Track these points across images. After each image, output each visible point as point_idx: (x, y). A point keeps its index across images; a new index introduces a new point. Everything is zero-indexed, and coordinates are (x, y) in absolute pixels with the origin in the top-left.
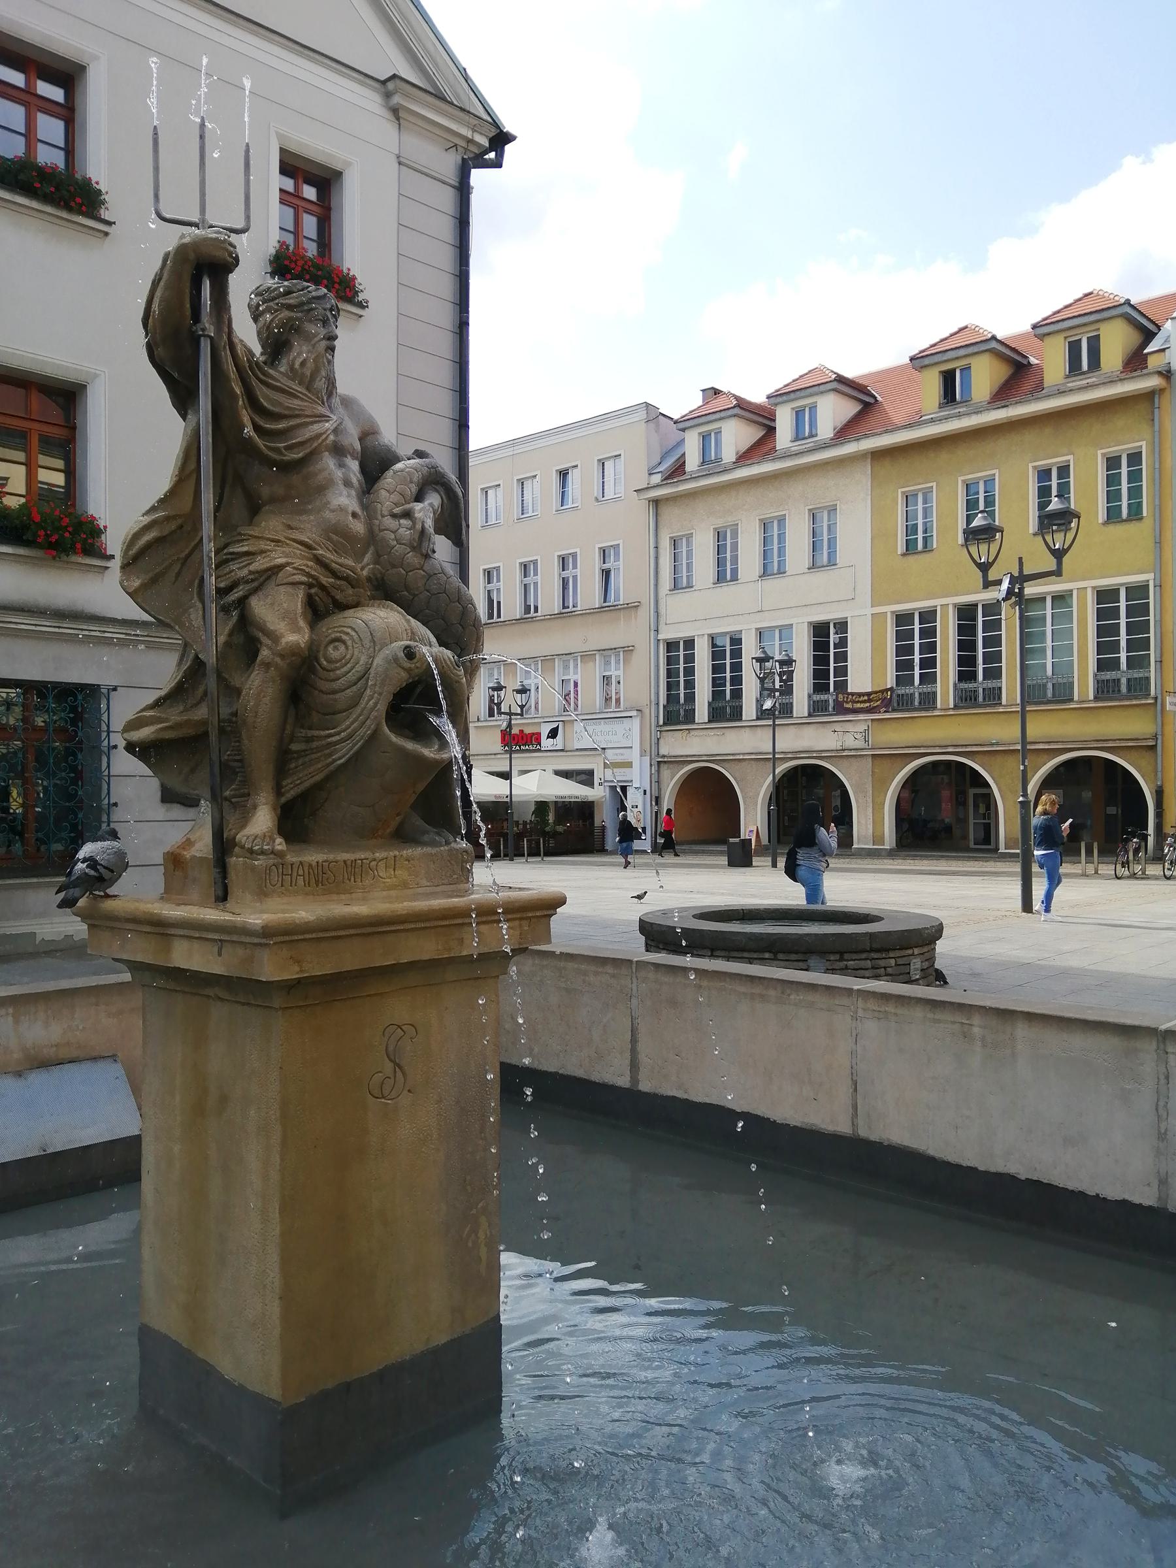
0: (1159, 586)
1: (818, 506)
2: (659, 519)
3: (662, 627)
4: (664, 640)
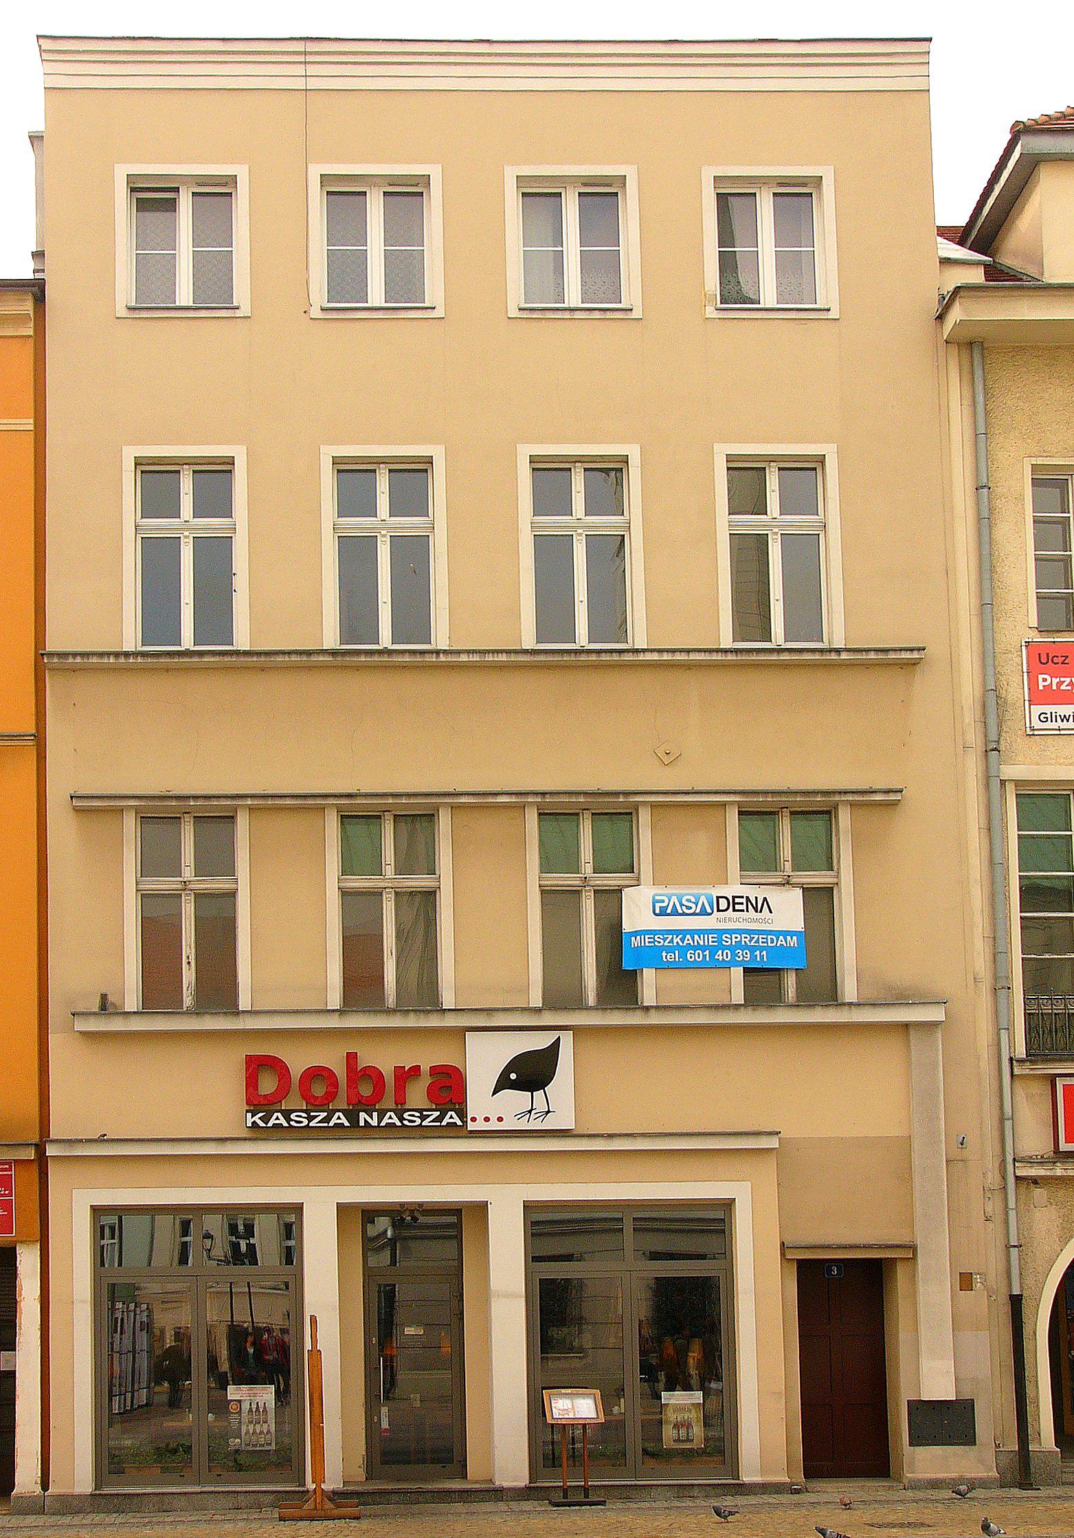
3: (1013, 740)
4: (1018, 783)
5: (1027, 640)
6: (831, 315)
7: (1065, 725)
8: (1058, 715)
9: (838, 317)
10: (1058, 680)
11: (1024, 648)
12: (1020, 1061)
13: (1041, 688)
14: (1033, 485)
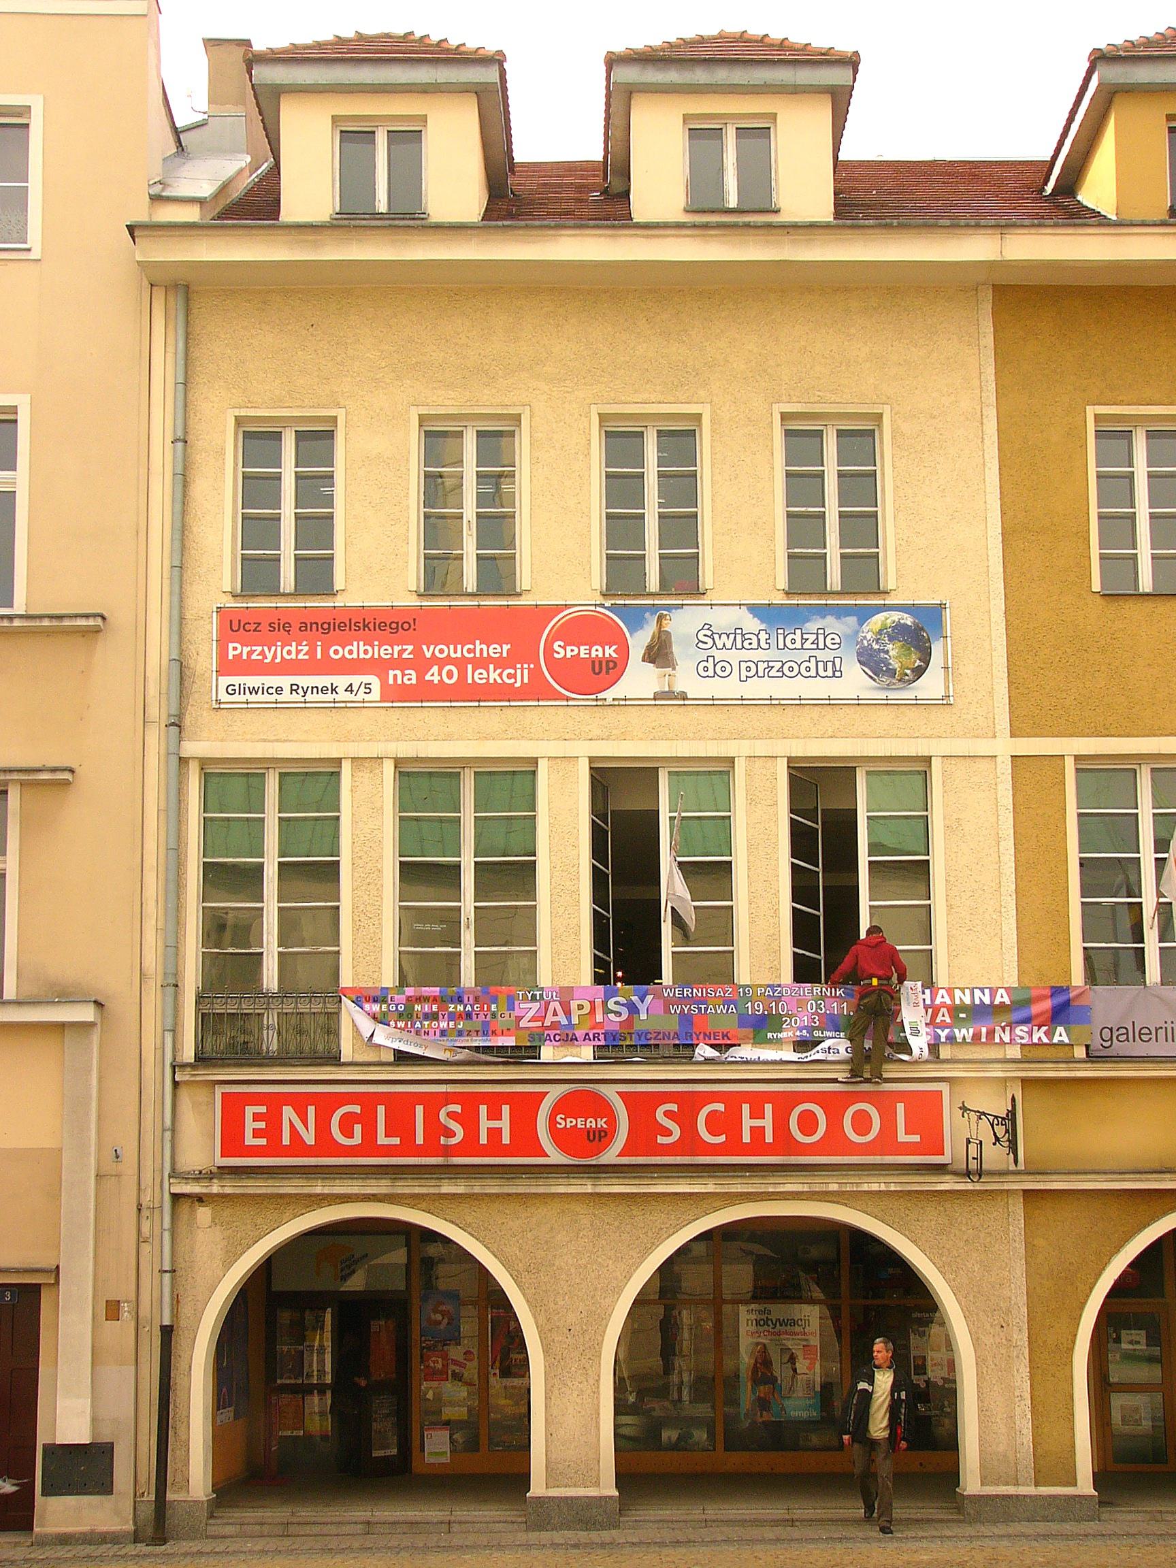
0: (917, 703)
1: (818, 409)
2: (195, 353)
3: (197, 714)
4: (204, 762)
5: (219, 606)
6: (32, 256)
7: (253, 698)
8: (246, 687)
9: (39, 258)
10: (249, 648)
11: (215, 614)
12: (184, 1066)
13: (230, 657)
14: (1097, 437)
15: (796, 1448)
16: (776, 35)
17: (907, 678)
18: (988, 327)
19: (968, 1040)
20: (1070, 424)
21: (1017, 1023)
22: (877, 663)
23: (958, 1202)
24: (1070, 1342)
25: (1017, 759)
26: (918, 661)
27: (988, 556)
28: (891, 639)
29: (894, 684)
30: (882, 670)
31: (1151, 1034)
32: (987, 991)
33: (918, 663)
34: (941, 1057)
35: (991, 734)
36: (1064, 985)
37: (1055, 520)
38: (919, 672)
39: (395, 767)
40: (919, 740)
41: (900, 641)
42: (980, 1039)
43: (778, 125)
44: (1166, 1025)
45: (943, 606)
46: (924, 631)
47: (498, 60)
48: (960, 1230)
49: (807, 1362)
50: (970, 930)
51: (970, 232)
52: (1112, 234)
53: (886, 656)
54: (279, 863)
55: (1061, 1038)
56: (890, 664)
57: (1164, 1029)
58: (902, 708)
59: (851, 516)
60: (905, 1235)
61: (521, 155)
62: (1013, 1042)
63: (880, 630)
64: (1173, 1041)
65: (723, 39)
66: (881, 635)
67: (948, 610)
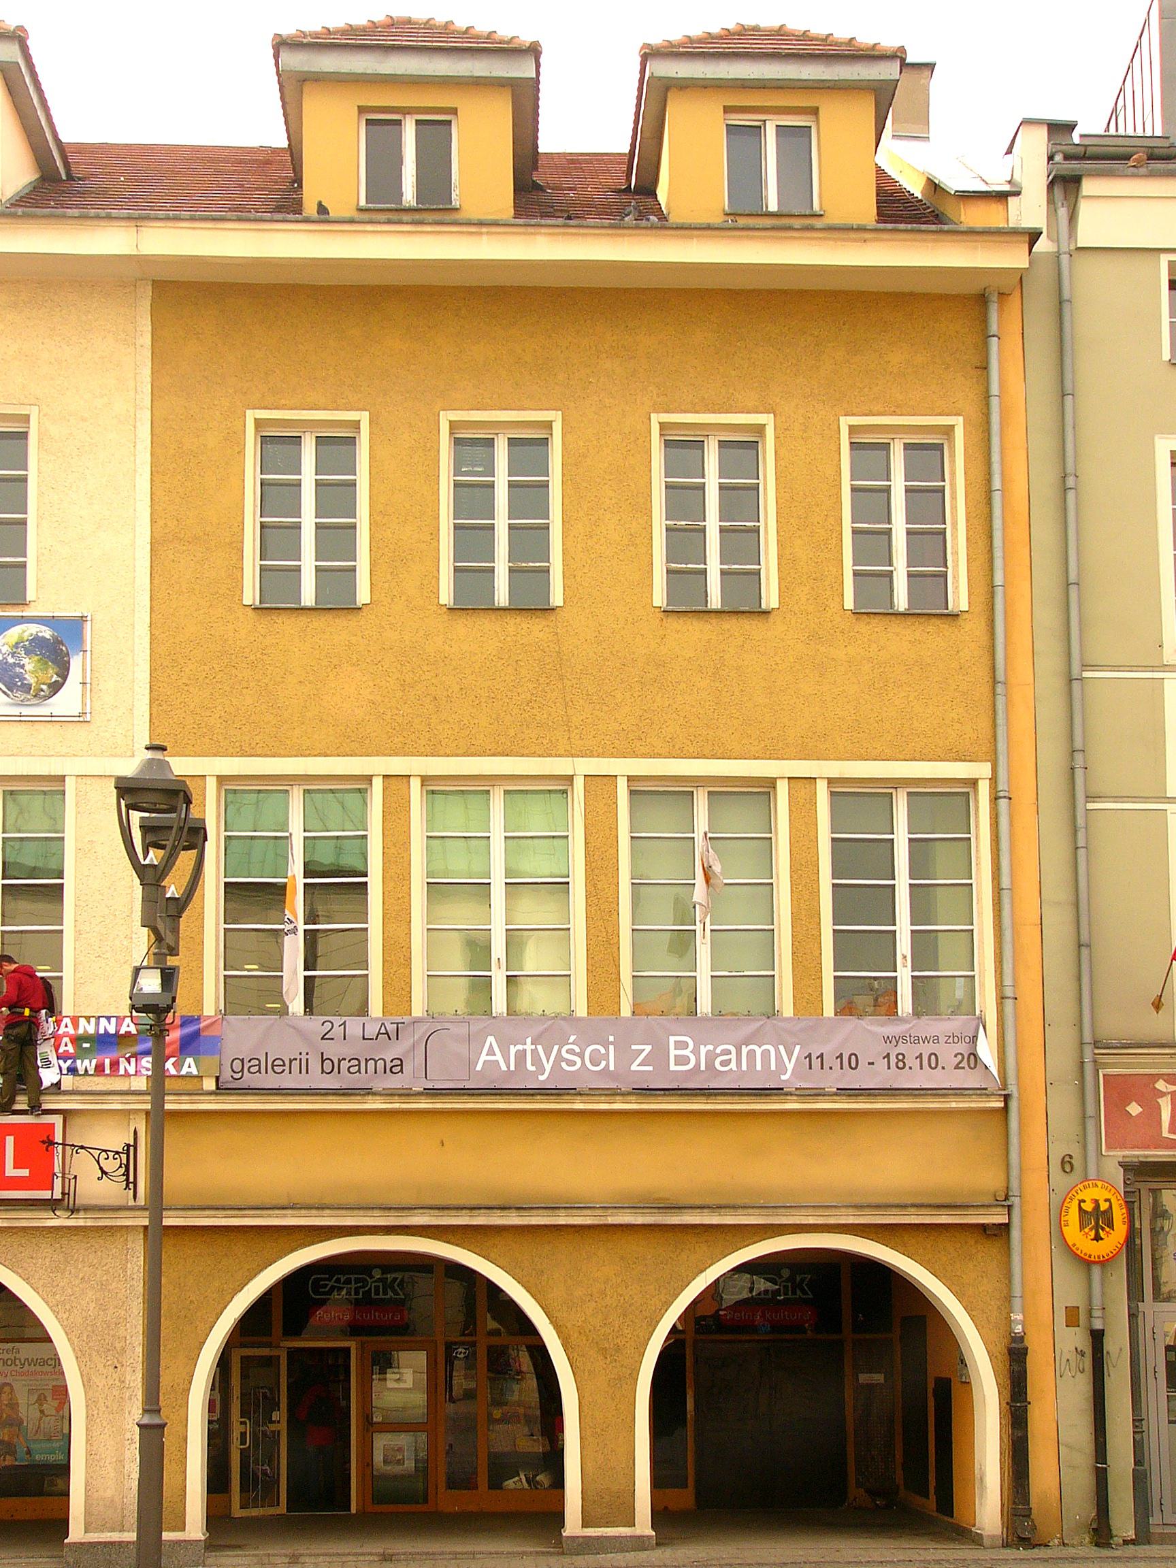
0: (52, 720)
14: (851, 449)
15: (41, 1493)
16: (461, 24)
17: (42, 693)
18: (145, 325)
19: (91, 1072)
20: (229, 428)
21: (141, 1054)
22: (12, 678)
23: (76, 1238)
24: (186, 1382)
25: (393, 780)
26: (55, 676)
27: (135, 567)
28: (28, 652)
29: (29, 700)
30: (15, 685)
31: (284, 1065)
32: (113, 1020)
33: (55, 678)
34: (62, 1089)
35: (129, 753)
36: (196, 1014)
37: (208, 529)
38: (56, 688)
39: (422, 785)
40: (53, 758)
41: (37, 655)
42: (104, 1071)
43: (821, 121)
44: (301, 1057)
45: (84, 619)
46: (63, 645)
47: (534, 51)
48: (76, 1267)
49: (56, 1403)
50: (99, 956)
51: (102, 224)
52: (310, 231)
53: (21, 670)
54: (305, 884)
55: (189, 1070)
56: (25, 679)
57: (298, 1060)
58: (37, 726)
59: (467, 528)
60: (17, 1273)
61: (544, 147)
62: (138, 1073)
63: (16, 643)
64: (307, 1073)
65: (393, 24)
66: (17, 648)
67: (89, 623)
